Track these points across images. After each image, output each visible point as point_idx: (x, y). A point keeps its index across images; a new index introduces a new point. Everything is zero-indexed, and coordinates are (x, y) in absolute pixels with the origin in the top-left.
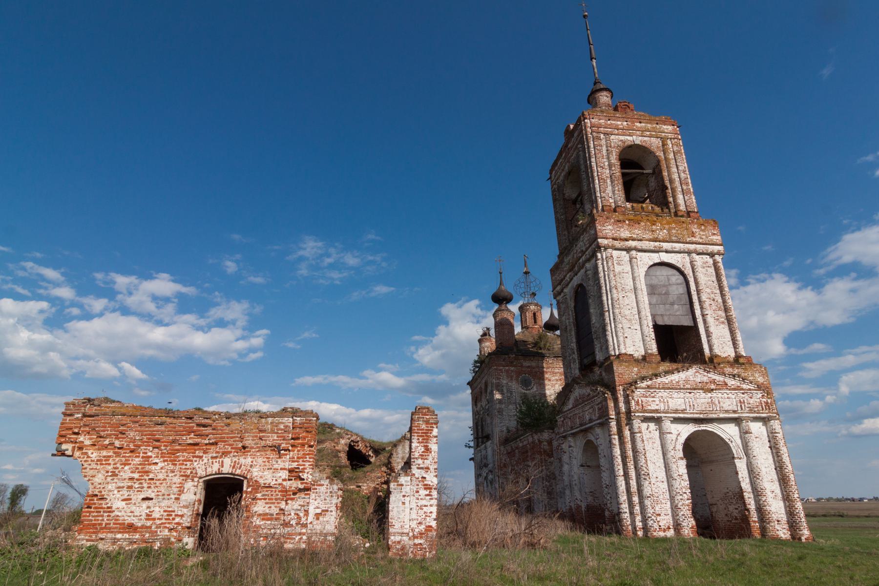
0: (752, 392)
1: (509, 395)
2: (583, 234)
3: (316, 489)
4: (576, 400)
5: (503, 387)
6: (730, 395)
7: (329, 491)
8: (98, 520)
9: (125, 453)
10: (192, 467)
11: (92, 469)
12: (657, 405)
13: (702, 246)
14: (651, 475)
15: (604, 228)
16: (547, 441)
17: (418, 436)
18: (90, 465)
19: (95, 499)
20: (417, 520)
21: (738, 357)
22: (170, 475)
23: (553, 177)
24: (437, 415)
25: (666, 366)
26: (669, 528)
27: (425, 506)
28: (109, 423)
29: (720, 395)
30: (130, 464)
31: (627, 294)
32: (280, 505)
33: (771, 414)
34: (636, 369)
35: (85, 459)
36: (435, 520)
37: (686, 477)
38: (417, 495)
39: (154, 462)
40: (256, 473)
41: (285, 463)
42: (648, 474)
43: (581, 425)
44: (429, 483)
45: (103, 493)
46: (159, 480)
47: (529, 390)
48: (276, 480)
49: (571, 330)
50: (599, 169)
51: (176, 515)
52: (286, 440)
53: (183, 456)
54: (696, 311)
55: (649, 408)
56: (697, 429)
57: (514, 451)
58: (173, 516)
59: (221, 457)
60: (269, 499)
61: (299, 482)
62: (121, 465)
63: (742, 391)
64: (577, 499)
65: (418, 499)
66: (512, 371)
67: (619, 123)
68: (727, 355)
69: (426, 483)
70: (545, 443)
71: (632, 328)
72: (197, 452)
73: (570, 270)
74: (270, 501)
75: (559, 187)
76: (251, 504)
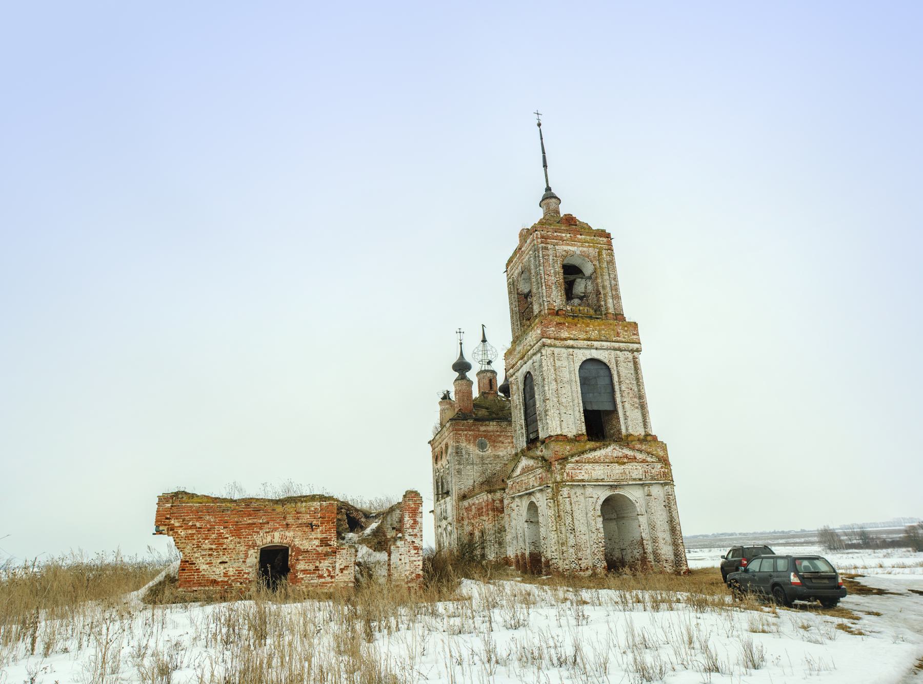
0: (654, 464)
1: (467, 457)
2: (531, 331)
3: (340, 552)
4: (523, 469)
5: (462, 449)
6: (638, 467)
7: (349, 553)
8: (191, 578)
9: (205, 531)
10: (252, 539)
11: (183, 543)
12: (583, 476)
13: (624, 344)
14: (576, 530)
15: (548, 330)
16: (500, 500)
17: (409, 513)
18: (180, 540)
19: (187, 563)
20: (410, 570)
21: (647, 435)
22: (238, 545)
23: (509, 271)
24: (421, 497)
25: (590, 445)
26: (587, 569)
27: (415, 561)
28: (190, 510)
29: (630, 467)
30: (209, 539)
31: (564, 385)
32: (315, 563)
33: (667, 481)
34: (568, 447)
35: (177, 536)
36: (422, 570)
37: (602, 530)
38: (409, 554)
39: (226, 536)
40: (297, 542)
41: (318, 534)
42: (574, 529)
43: (526, 489)
44: (417, 545)
45: (192, 559)
46: (231, 549)
47: (485, 452)
48: (312, 547)
49: (520, 409)
50: (546, 276)
51: (244, 573)
52: (316, 518)
53: (246, 532)
54: (617, 399)
55: (577, 478)
56: (611, 494)
57: (471, 507)
58: (243, 574)
59: (272, 531)
60: (308, 560)
61: (328, 547)
62: (202, 539)
63: (646, 464)
64: (522, 548)
65: (410, 556)
66: (470, 435)
67: (564, 235)
68: (638, 434)
69: (415, 545)
70: (498, 502)
71: (567, 413)
72: (255, 529)
73: (522, 358)
74: (309, 561)
75: (514, 282)
76: (295, 563)
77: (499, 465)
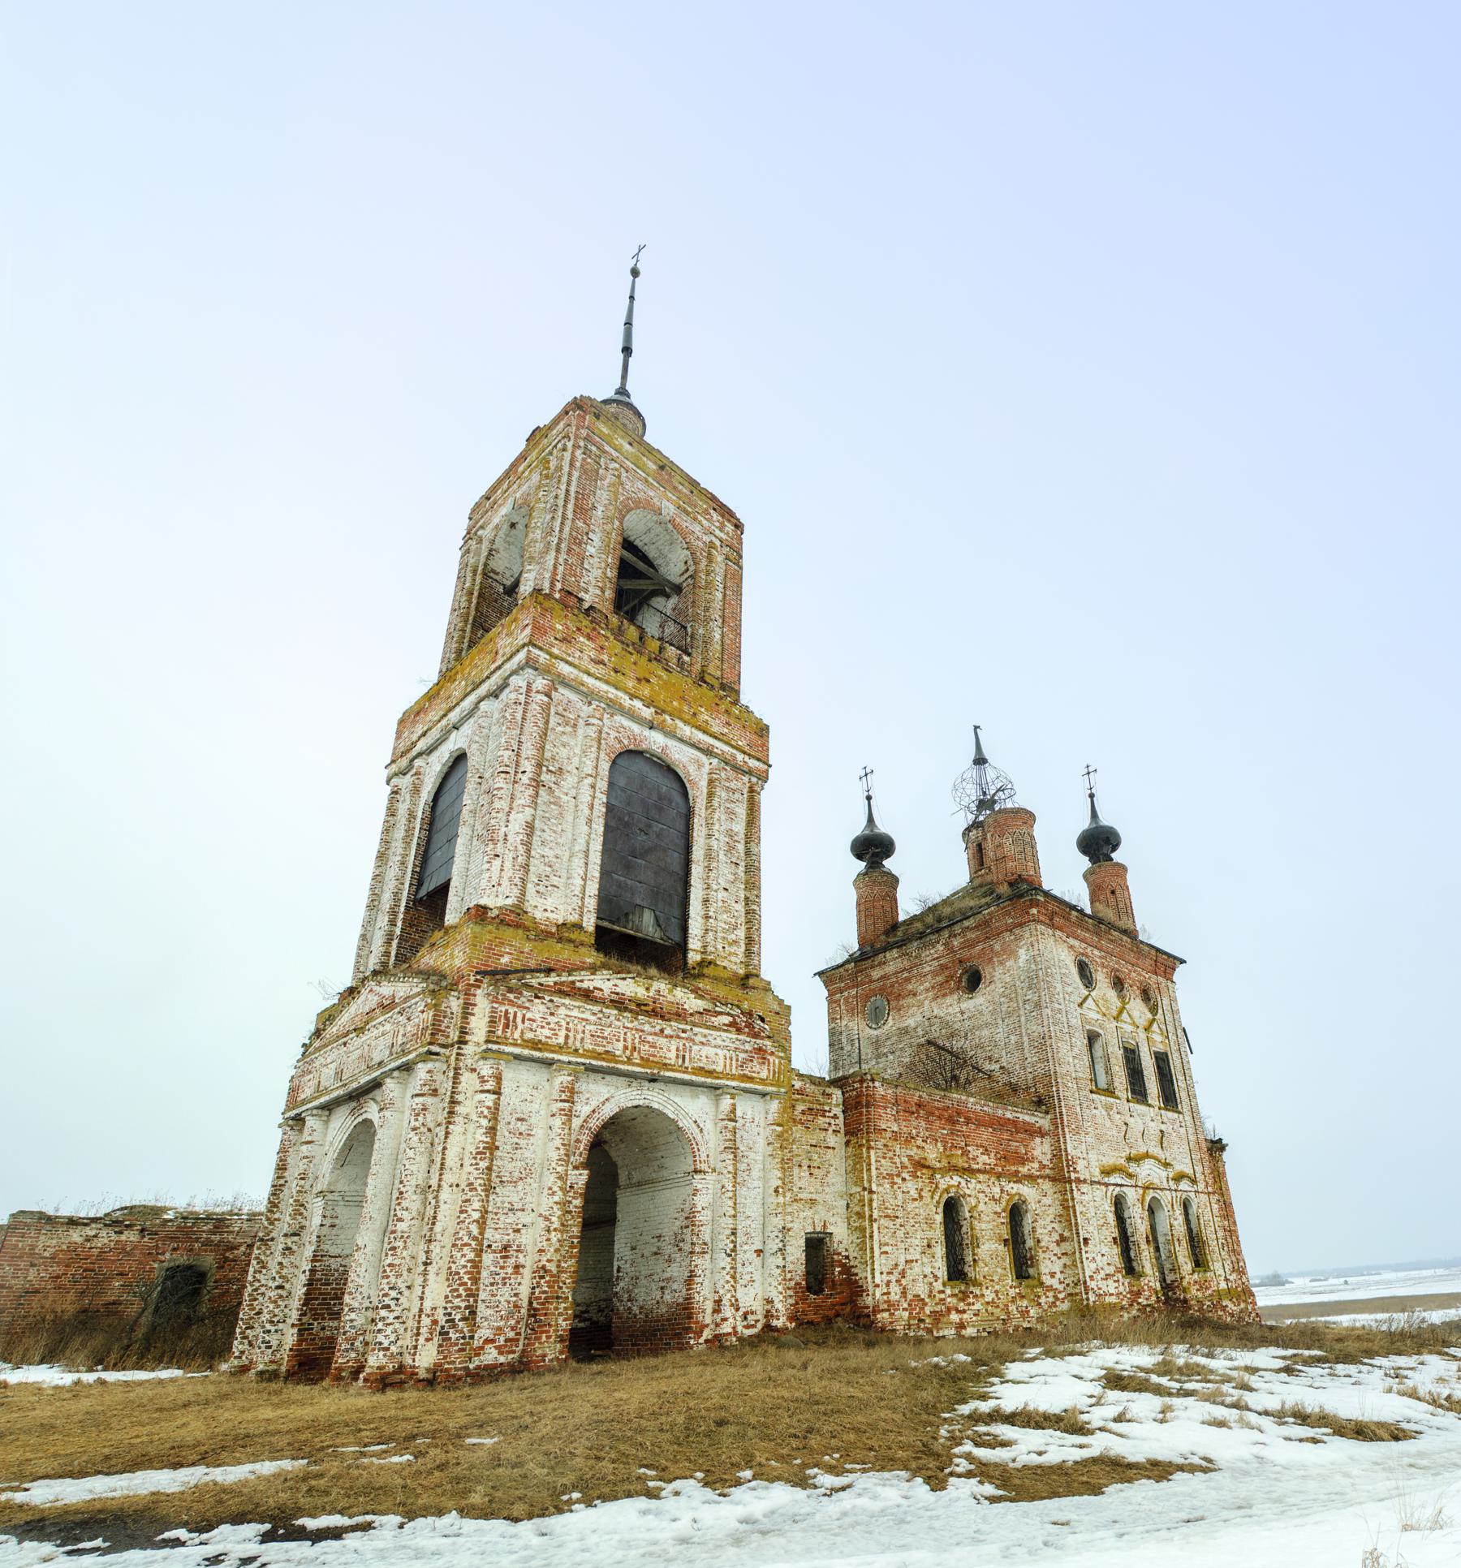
77: (909, 1051)
